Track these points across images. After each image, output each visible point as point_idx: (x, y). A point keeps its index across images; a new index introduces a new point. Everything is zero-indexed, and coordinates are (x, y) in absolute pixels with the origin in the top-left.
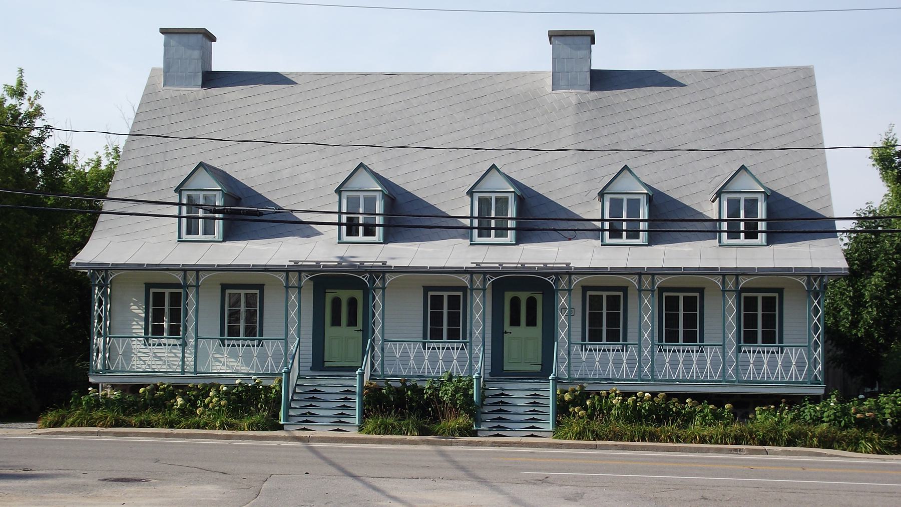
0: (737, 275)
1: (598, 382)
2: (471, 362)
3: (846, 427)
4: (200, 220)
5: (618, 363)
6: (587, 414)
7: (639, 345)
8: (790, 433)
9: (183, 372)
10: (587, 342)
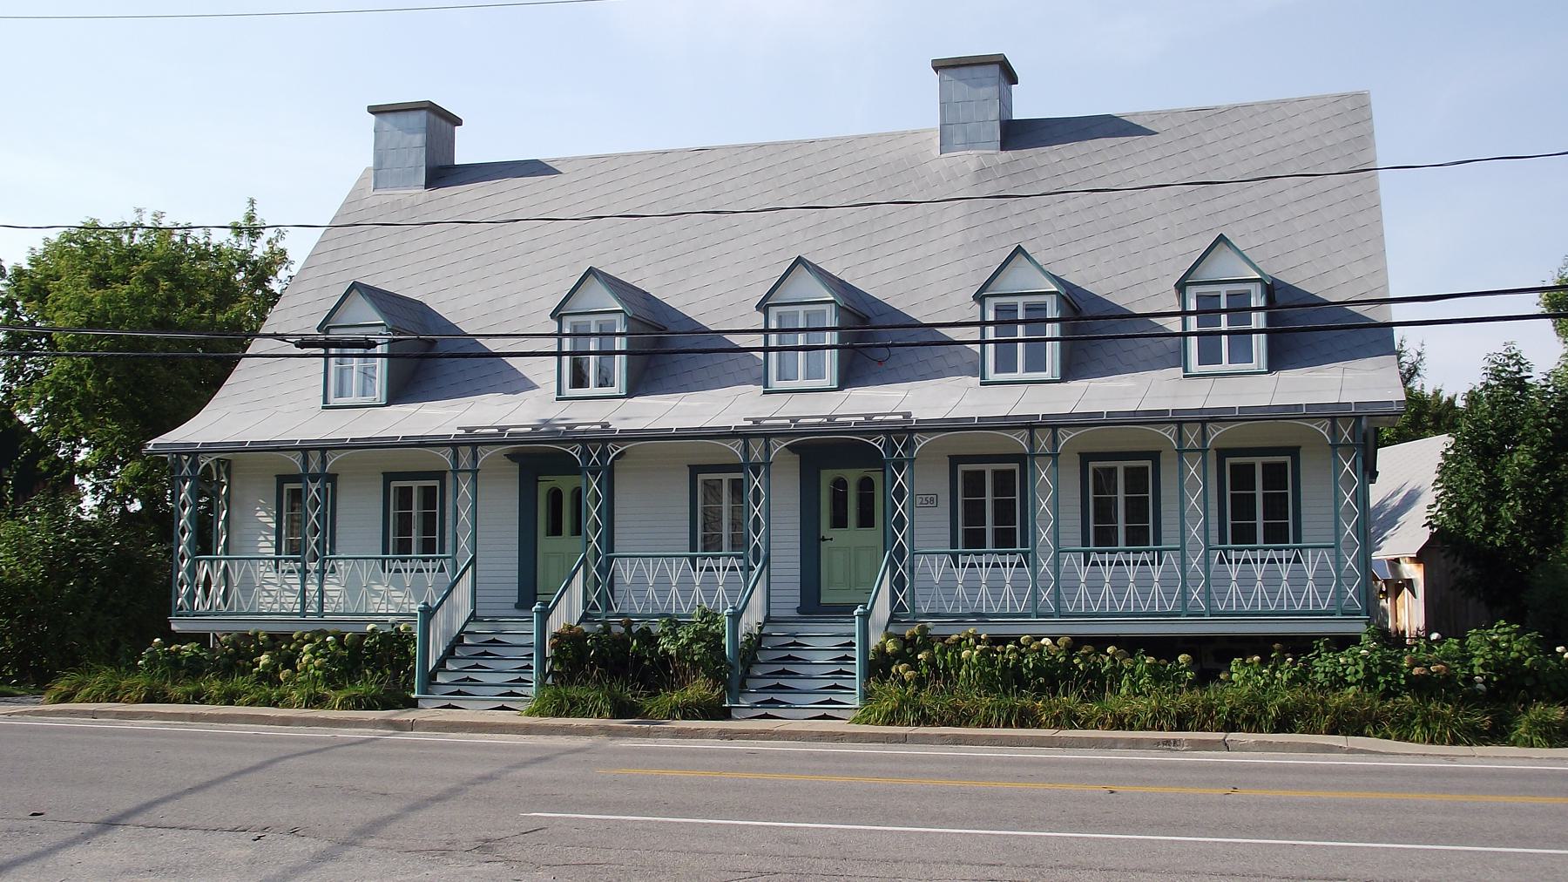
0: (1204, 422)
1: (960, 619)
2: (1035, 587)
3: (1387, 694)
4: (1224, 338)
5: (1144, 585)
6: (924, 679)
7: (1182, 549)
8: (1282, 707)
9: (303, 613)
10: (1229, 545)
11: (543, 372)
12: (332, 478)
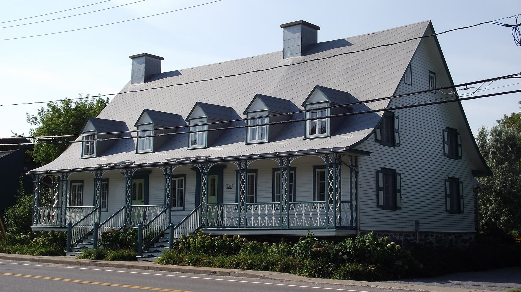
11: (201, 136)
12: (294, 169)
